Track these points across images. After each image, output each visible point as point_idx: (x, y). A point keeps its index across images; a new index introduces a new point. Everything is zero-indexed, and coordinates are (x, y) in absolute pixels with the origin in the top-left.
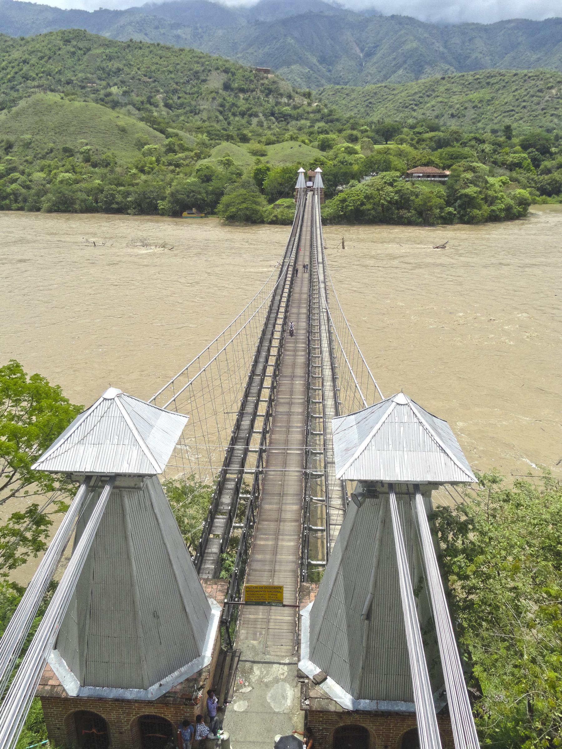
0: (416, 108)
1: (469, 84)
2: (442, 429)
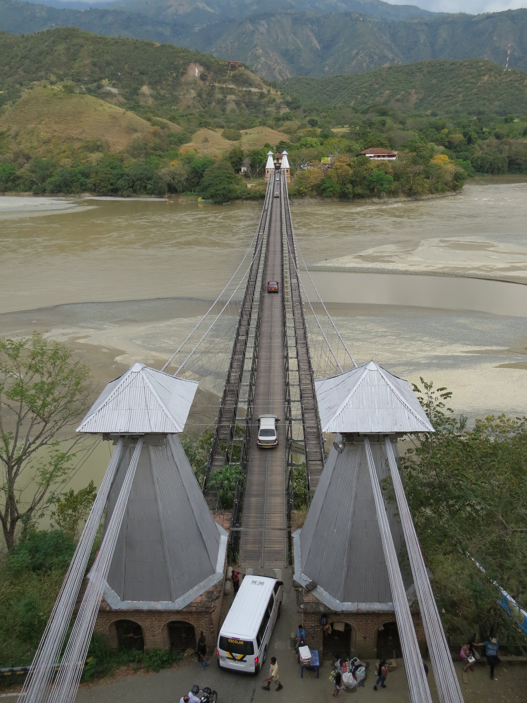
0: (367, 94)
1: (413, 73)
2: (404, 389)
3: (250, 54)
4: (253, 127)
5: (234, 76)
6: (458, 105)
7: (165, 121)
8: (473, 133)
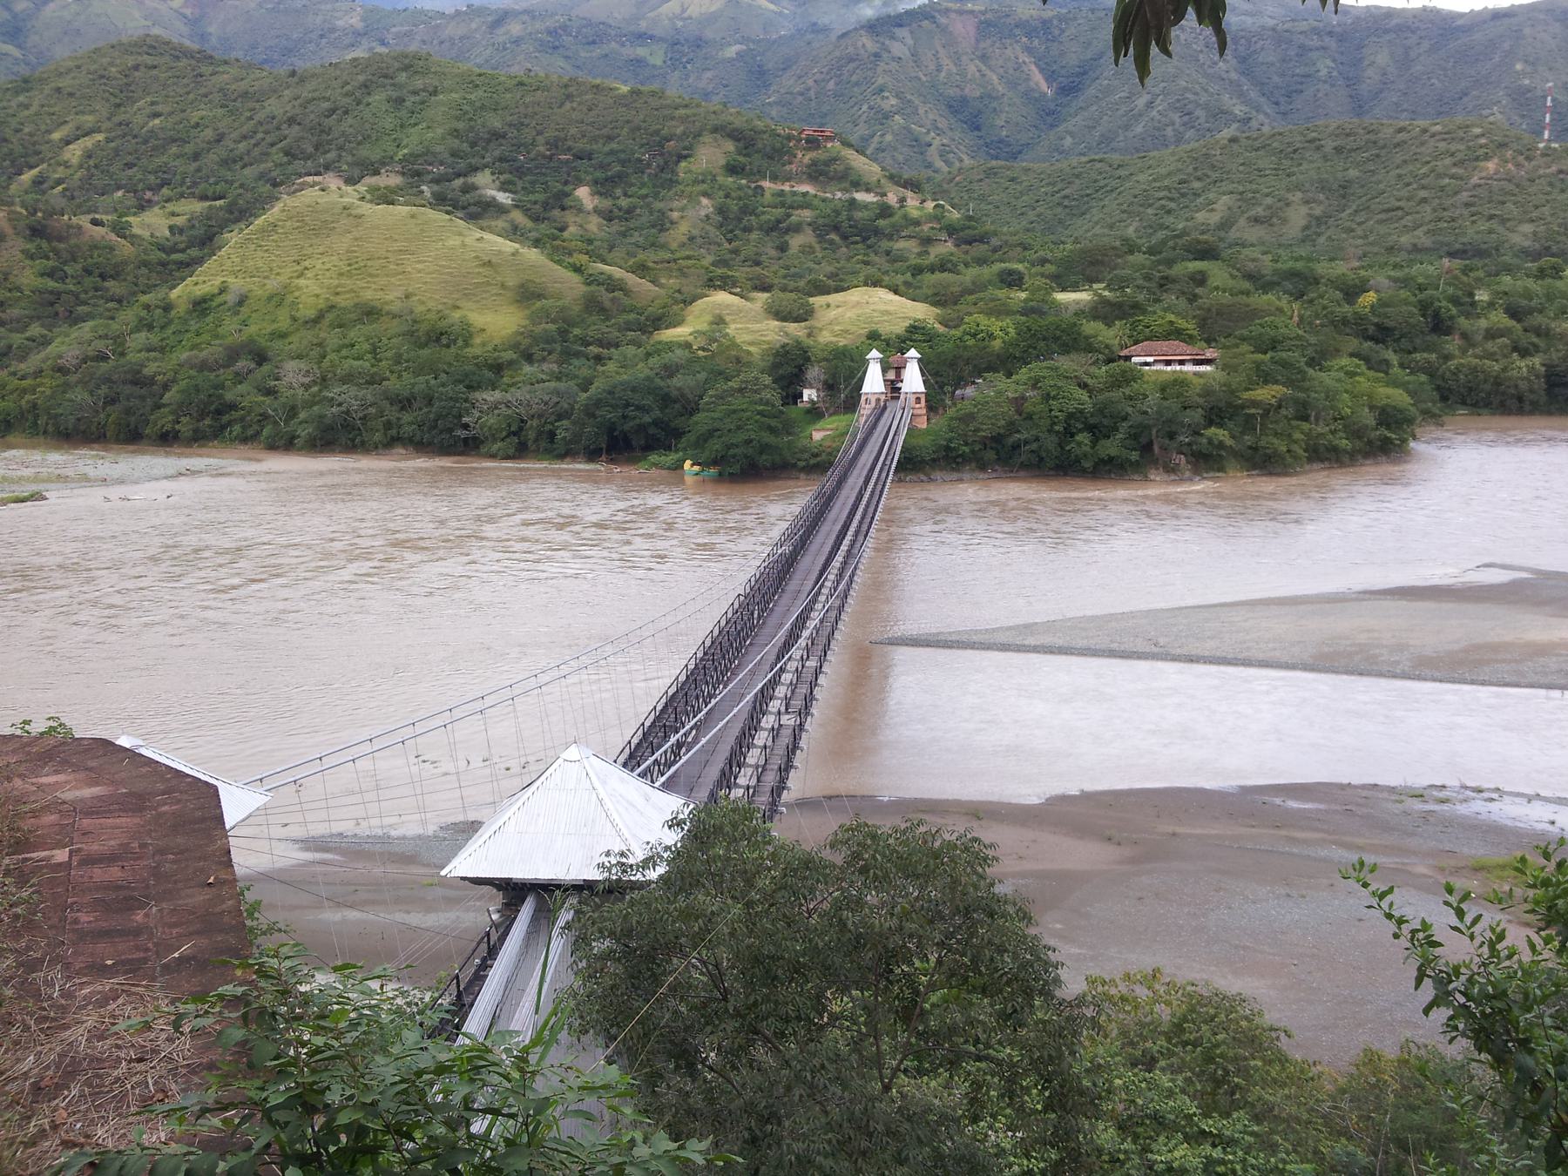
0: (1173, 205)
1: (1295, 151)
3: (865, 108)
4: (849, 288)
5: (814, 163)
6: (1419, 232)
7: (617, 272)
8: (1444, 303)
